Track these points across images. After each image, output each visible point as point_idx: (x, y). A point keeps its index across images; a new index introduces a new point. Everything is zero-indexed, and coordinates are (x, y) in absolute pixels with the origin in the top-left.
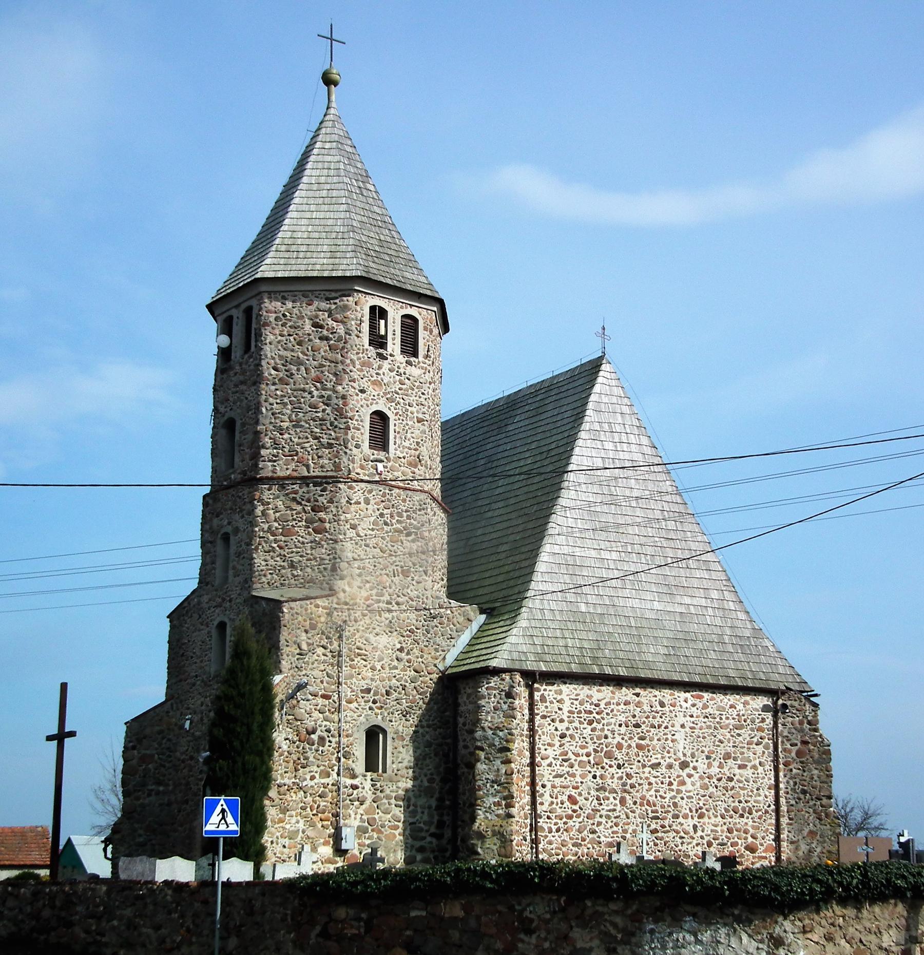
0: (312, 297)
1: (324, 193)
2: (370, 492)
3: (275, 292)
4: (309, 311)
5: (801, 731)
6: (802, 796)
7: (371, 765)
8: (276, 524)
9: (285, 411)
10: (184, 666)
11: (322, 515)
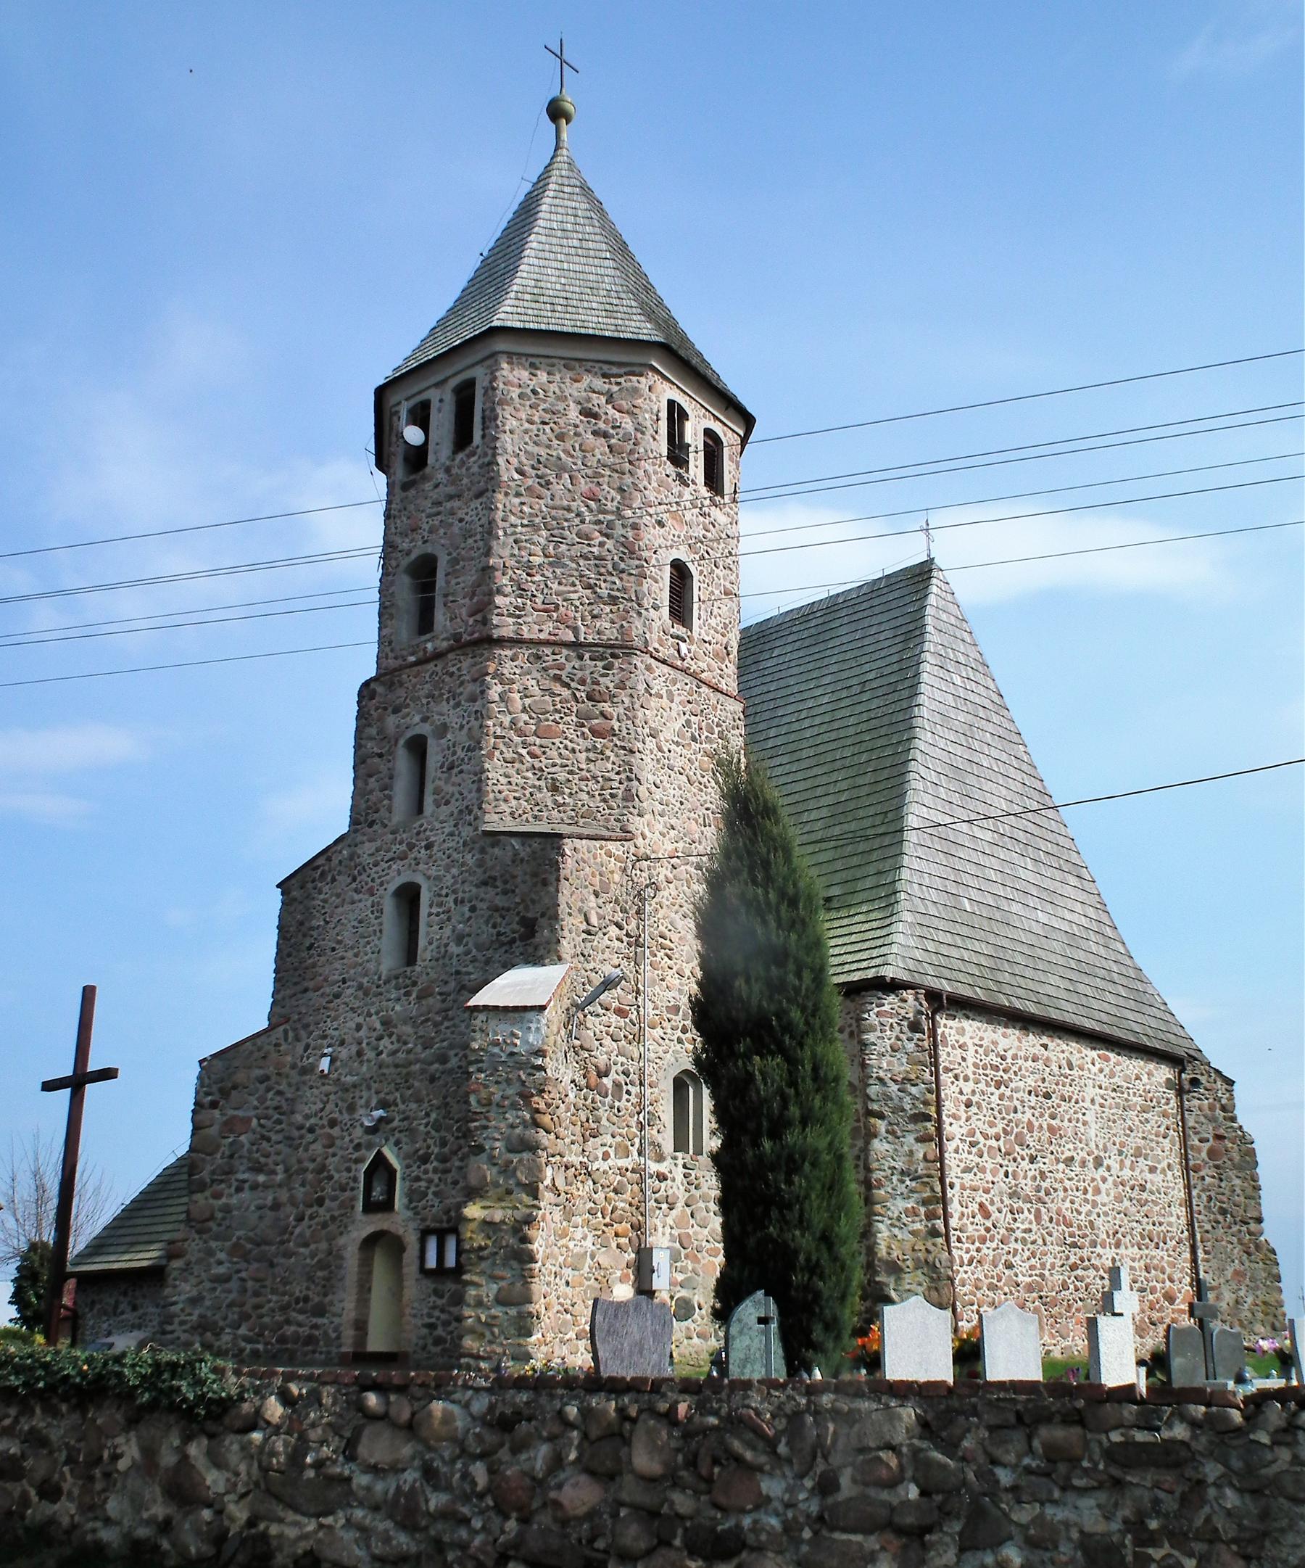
0: (581, 370)
1: (576, 243)
2: (674, 682)
3: (520, 355)
4: (576, 390)
5: (1212, 1119)
6: (1220, 1218)
7: (680, 1145)
8: (525, 717)
9: (536, 538)
10: (314, 965)
11: (606, 707)
